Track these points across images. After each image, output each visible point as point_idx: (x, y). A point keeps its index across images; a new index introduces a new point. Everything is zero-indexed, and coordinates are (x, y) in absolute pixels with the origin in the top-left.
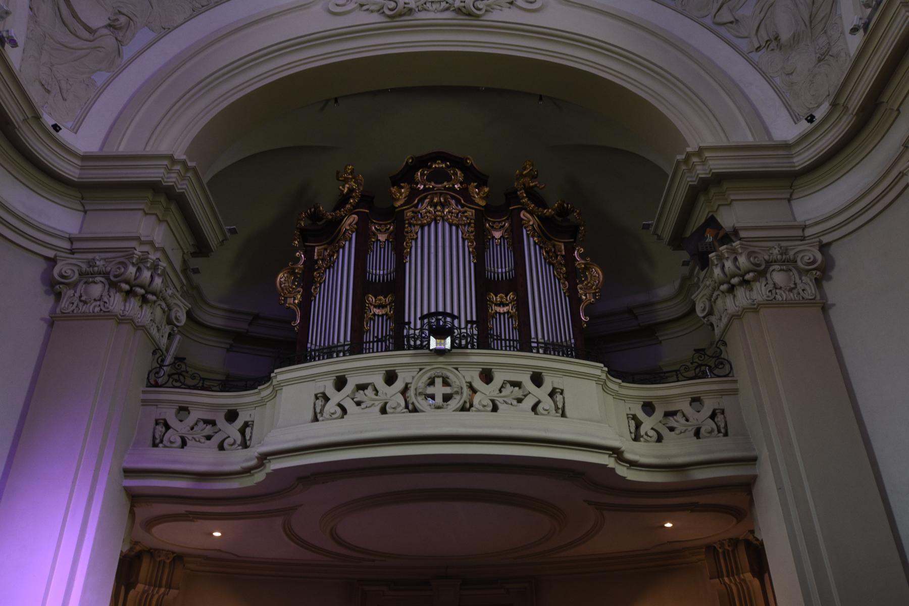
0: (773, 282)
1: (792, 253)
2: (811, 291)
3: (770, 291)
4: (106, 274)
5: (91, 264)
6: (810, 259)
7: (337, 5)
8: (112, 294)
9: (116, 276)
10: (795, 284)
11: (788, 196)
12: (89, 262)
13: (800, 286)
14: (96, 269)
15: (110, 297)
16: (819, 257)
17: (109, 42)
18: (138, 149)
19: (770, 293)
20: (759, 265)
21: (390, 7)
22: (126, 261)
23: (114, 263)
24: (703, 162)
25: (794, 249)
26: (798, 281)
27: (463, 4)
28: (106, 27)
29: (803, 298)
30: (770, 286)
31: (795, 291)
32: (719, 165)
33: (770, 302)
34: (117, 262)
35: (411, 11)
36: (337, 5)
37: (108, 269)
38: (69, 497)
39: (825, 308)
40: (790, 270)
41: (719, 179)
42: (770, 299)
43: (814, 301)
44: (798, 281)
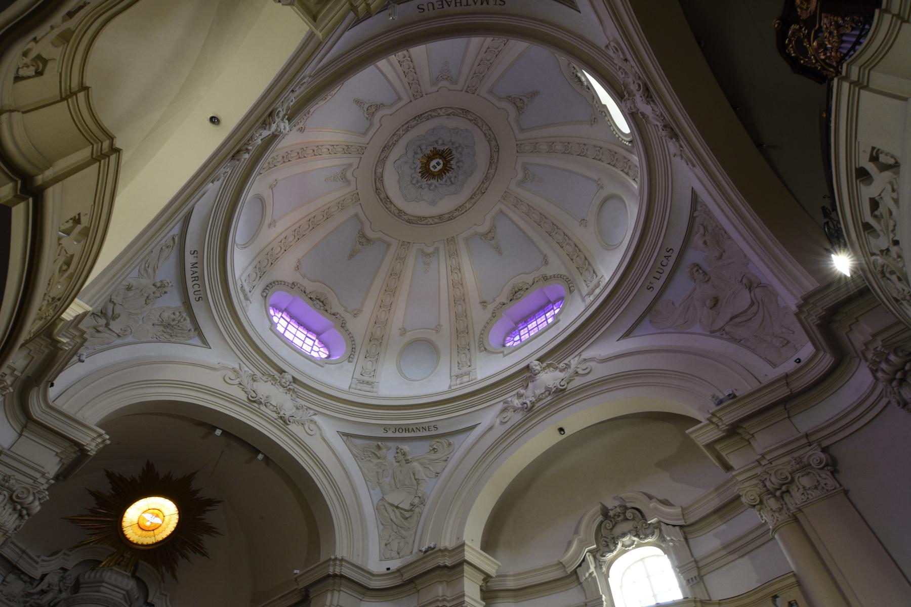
0: (802, 485)
1: (805, 460)
2: (831, 482)
3: (803, 494)
4: (11, 491)
5: (6, 478)
6: (817, 460)
7: (230, 378)
8: (7, 507)
9: (17, 497)
10: (818, 481)
11: (787, 416)
12: (5, 476)
13: (822, 482)
14: (7, 484)
15: (4, 509)
16: (823, 456)
17: (758, 292)
18: (71, 412)
19: (803, 495)
20: (787, 478)
21: (252, 396)
22: (31, 490)
23: (20, 485)
24: (341, 565)
25: (805, 456)
26: (819, 479)
27: (284, 415)
28: (750, 291)
29: (827, 490)
30: (801, 490)
31: (820, 488)
32: (347, 571)
33: (805, 503)
34: (24, 486)
35: (261, 403)
36: (230, 378)
37: (15, 489)
38: (736, 318)
39: (846, 492)
40: (809, 473)
41: (342, 576)
42: (804, 500)
43: (836, 490)
44: (819, 479)
